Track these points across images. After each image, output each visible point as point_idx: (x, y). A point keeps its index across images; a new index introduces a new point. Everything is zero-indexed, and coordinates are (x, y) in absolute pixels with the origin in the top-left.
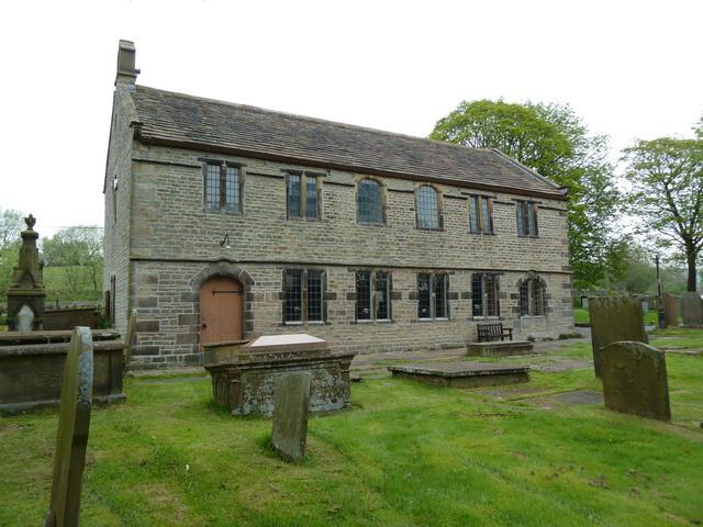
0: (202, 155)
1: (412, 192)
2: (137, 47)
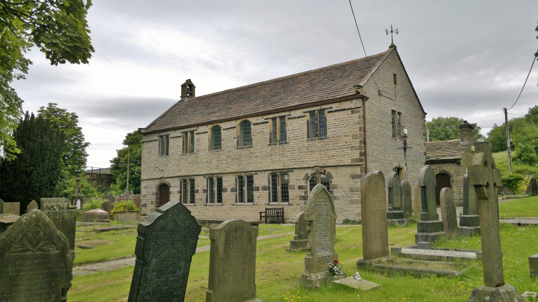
0: (158, 135)
1: (235, 127)
2: (194, 82)
